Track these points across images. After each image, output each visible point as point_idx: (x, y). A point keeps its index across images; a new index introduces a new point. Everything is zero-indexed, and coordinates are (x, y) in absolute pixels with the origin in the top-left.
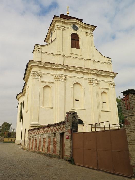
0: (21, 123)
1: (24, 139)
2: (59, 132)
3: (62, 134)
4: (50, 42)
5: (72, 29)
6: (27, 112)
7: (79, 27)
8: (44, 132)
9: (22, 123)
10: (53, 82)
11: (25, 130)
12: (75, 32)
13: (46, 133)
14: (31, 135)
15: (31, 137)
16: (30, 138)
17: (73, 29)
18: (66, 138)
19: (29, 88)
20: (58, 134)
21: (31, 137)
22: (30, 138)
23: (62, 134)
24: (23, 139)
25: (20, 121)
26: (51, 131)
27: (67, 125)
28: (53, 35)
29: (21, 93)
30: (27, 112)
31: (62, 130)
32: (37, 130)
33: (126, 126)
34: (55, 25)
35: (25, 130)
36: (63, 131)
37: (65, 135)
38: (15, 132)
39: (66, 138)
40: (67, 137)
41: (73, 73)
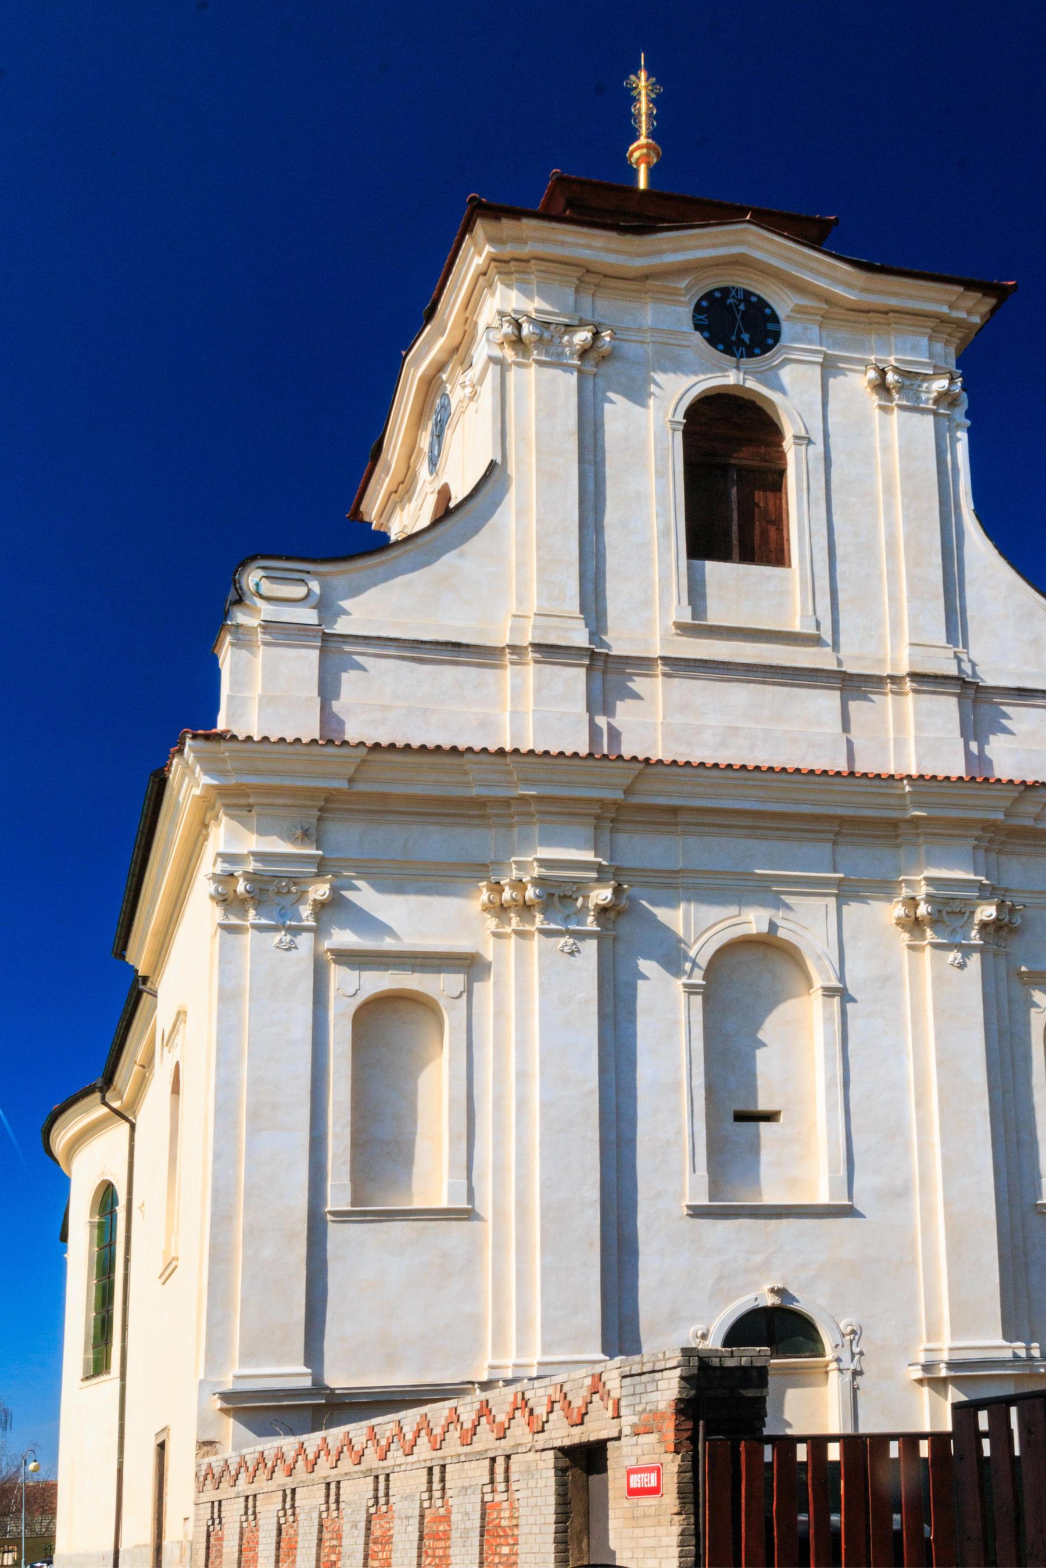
0: (109, 1383)
1: (147, 1536)
2: (541, 1440)
3: (584, 1461)
4: (425, 521)
5: (697, 338)
6: (168, 1272)
7: (782, 312)
8: (371, 1458)
9: (117, 1383)
10: (462, 945)
11: (162, 1446)
12: (730, 377)
13: (396, 1455)
14: (226, 1491)
15: (233, 1511)
16: (216, 1516)
17: (712, 341)
18: (633, 1492)
19: (187, 1030)
20: (531, 1456)
21: (233, 1511)
22: (216, 1516)
23: (584, 1461)
24: (138, 1532)
25: (98, 1366)
26: (454, 1434)
27: (636, 1369)
28: (452, 438)
29: (97, 1095)
30: (168, 1272)
31: (576, 1417)
32: (319, 1435)
33: (157, 780)
34: (483, 322)
35: (162, 1446)
36: (594, 1430)
37: (620, 1460)
38: (46, 1483)
39: (633, 1492)
40: (636, 1481)
41: (494, 422)
